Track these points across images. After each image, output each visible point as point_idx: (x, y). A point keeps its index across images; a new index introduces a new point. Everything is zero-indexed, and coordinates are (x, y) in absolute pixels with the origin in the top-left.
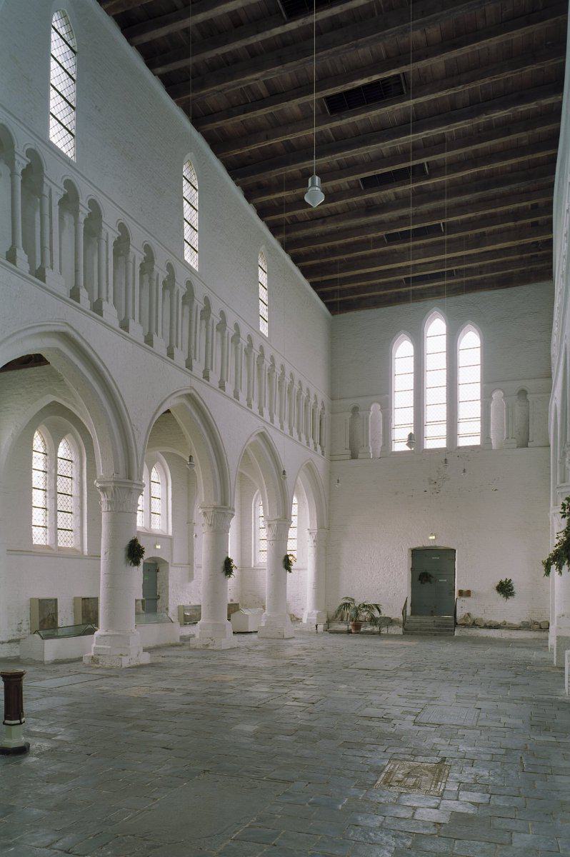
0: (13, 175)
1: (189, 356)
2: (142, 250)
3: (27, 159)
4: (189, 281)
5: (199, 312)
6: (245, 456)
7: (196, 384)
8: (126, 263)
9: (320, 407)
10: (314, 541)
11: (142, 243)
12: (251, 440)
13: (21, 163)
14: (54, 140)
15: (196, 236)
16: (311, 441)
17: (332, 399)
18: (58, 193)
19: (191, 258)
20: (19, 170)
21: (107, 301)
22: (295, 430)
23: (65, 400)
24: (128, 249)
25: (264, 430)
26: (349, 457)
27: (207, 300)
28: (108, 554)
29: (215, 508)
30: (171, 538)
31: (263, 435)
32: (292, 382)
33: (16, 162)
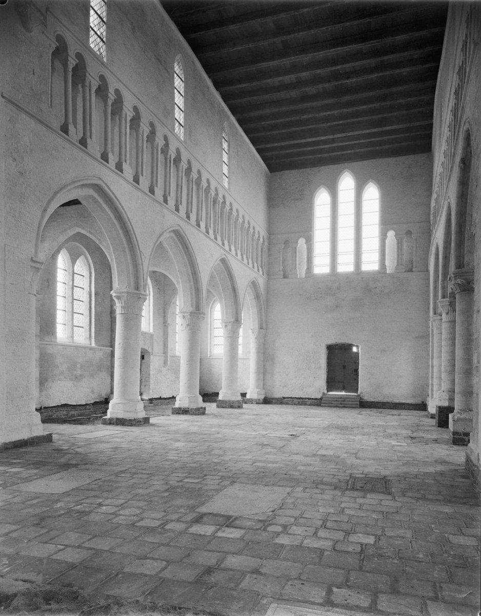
0: (66, 72)
1: (137, 172)
2: (132, 110)
3: (76, 60)
4: (177, 148)
5: (184, 170)
6: (212, 277)
7: (182, 224)
8: (120, 120)
9: (261, 240)
10: (256, 338)
11: (148, 120)
12: (216, 264)
13: (72, 62)
14: (92, 46)
15: (183, 115)
16: (256, 265)
17: (270, 235)
18: (95, 83)
19: (179, 131)
20: (71, 67)
21: (126, 162)
22: (245, 256)
23: (90, 232)
24: (139, 125)
25: (225, 257)
26: (282, 277)
27: (189, 162)
28: (121, 344)
29: (191, 313)
30: (152, 335)
31: (223, 261)
32: (244, 222)
33: (69, 62)
